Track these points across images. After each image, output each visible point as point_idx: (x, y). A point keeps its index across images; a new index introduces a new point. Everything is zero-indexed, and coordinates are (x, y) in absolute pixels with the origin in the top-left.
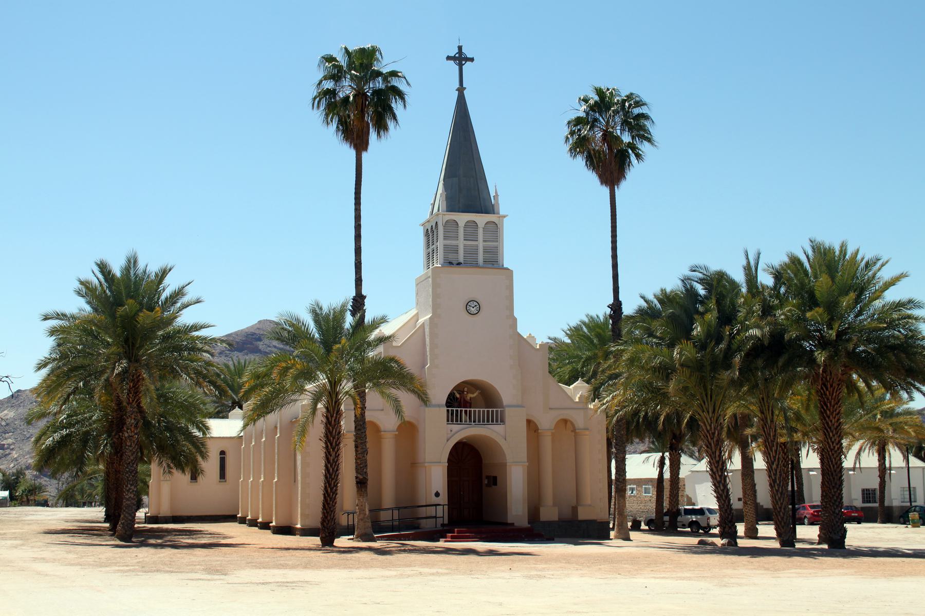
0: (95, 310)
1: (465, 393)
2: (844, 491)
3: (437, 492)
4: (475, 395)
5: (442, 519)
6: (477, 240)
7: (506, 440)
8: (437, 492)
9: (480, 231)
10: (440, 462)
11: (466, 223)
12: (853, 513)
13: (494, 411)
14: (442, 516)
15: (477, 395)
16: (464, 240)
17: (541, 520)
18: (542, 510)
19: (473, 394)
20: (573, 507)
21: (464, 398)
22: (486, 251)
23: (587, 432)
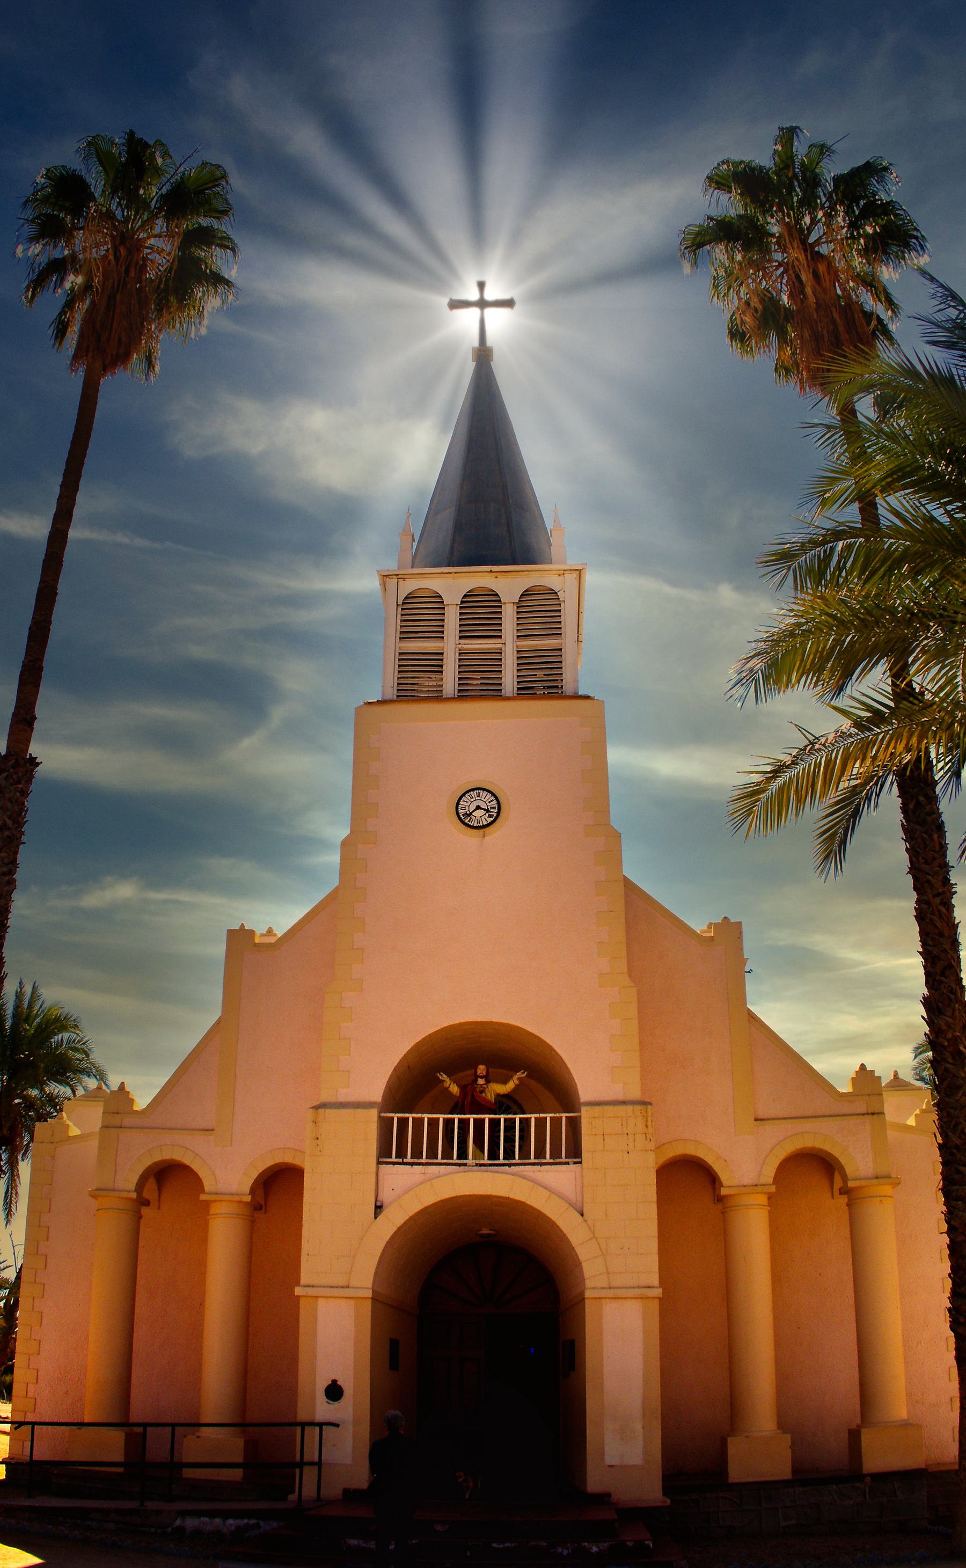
0: (495, 1103)
1: (481, 1081)
2: (130, 1414)
3: (334, 1382)
4: (511, 1086)
5: (316, 1467)
6: (500, 637)
7: (582, 1215)
8: (334, 1382)
9: (509, 615)
10: (348, 1287)
11: (465, 596)
12: (833, 198)
13: (514, 1120)
14: (316, 1459)
15: (517, 1086)
16: (461, 638)
17: (731, 1480)
18: (735, 1447)
19: (505, 1082)
20: (850, 1431)
21: (473, 1096)
22: (524, 660)
23: (887, 1190)
